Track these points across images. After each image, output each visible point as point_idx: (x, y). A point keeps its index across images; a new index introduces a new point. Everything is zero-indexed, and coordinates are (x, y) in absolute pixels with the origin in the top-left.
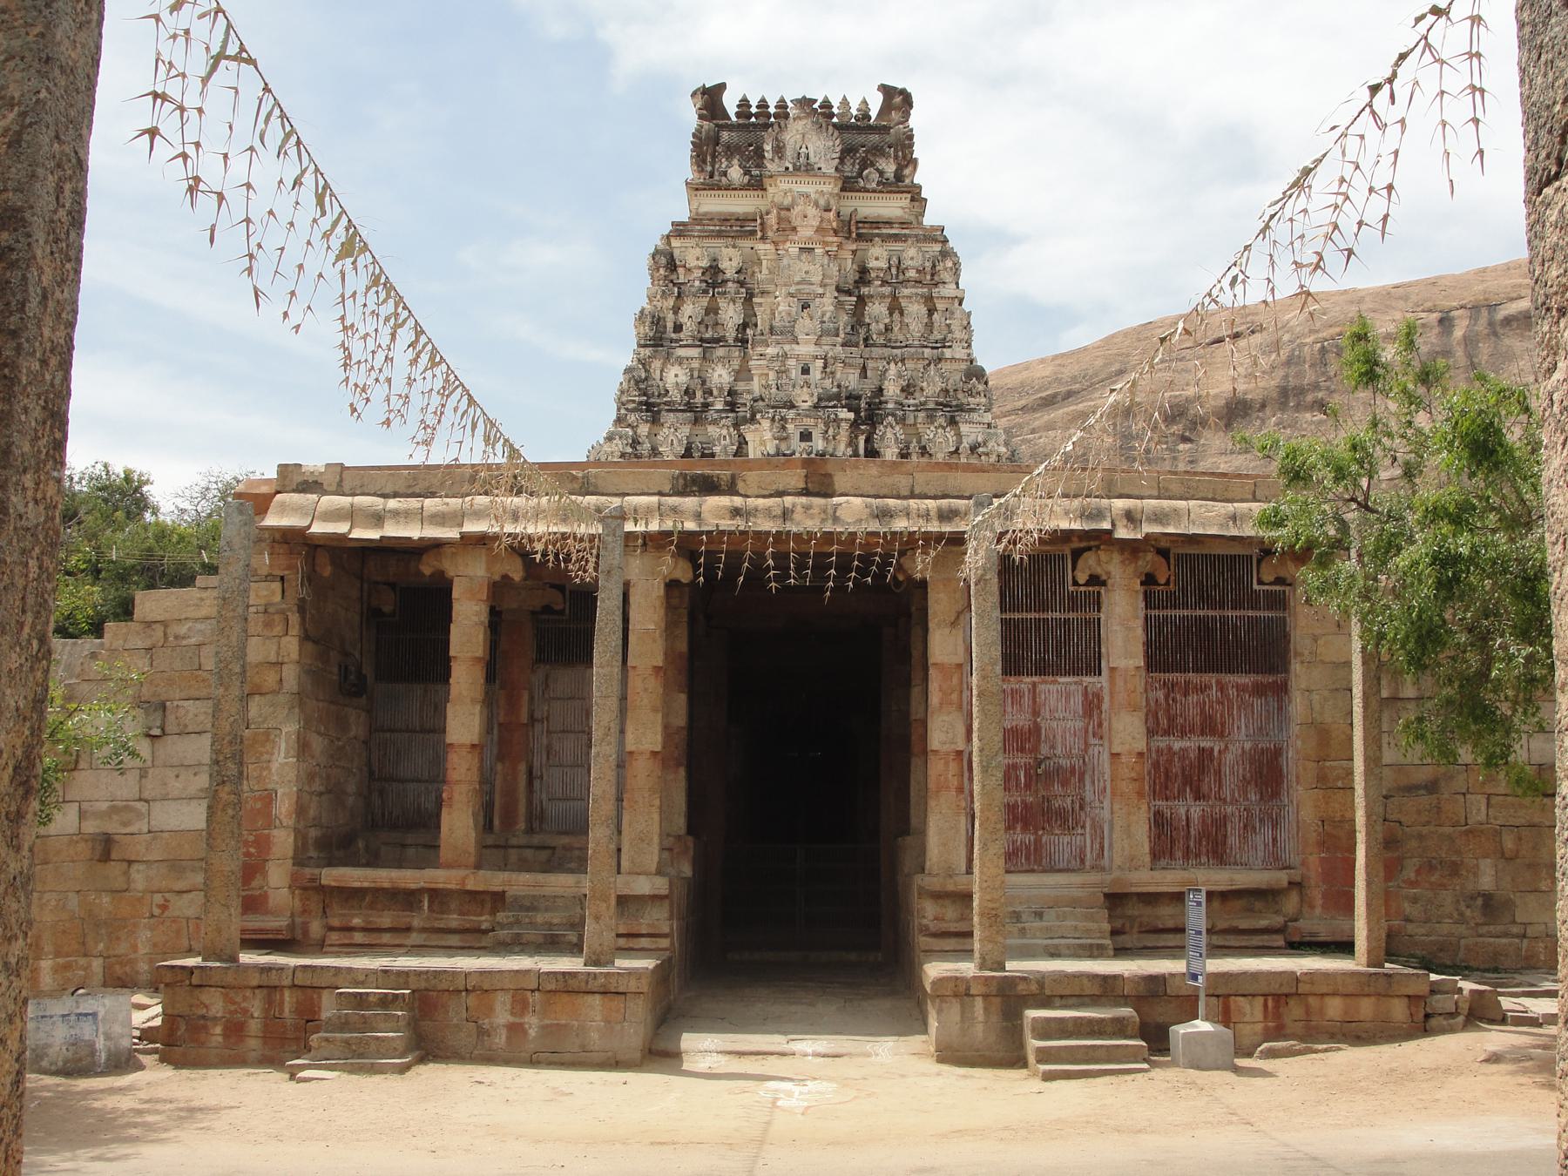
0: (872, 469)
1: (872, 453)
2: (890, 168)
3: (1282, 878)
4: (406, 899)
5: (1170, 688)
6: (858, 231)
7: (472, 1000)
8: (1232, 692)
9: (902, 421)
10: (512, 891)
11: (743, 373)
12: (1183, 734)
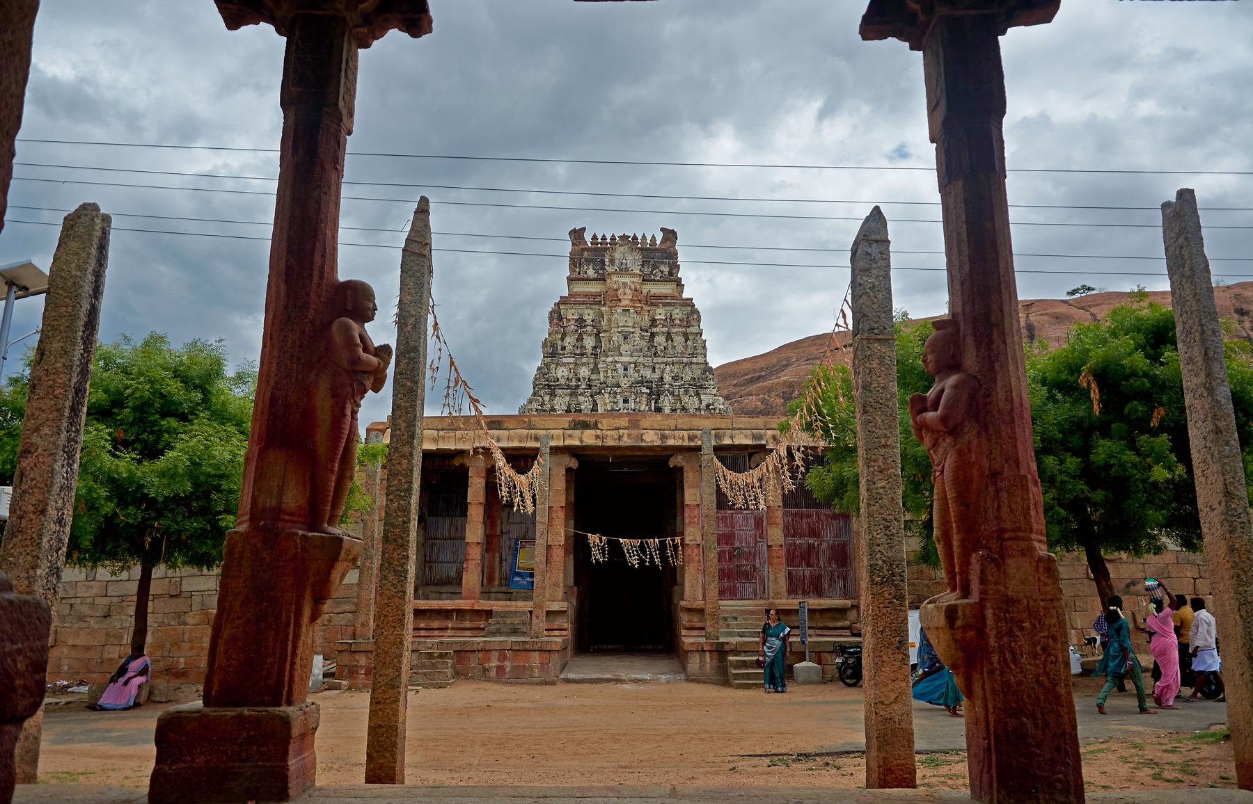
0: (659, 417)
1: (658, 410)
2: (666, 270)
3: (849, 603)
4: (445, 614)
5: (795, 516)
6: (653, 301)
7: (480, 655)
8: (823, 518)
9: (672, 394)
10: (494, 609)
11: (595, 370)
12: (801, 537)
